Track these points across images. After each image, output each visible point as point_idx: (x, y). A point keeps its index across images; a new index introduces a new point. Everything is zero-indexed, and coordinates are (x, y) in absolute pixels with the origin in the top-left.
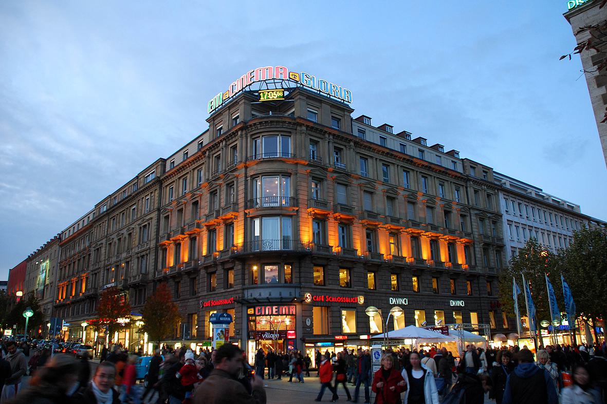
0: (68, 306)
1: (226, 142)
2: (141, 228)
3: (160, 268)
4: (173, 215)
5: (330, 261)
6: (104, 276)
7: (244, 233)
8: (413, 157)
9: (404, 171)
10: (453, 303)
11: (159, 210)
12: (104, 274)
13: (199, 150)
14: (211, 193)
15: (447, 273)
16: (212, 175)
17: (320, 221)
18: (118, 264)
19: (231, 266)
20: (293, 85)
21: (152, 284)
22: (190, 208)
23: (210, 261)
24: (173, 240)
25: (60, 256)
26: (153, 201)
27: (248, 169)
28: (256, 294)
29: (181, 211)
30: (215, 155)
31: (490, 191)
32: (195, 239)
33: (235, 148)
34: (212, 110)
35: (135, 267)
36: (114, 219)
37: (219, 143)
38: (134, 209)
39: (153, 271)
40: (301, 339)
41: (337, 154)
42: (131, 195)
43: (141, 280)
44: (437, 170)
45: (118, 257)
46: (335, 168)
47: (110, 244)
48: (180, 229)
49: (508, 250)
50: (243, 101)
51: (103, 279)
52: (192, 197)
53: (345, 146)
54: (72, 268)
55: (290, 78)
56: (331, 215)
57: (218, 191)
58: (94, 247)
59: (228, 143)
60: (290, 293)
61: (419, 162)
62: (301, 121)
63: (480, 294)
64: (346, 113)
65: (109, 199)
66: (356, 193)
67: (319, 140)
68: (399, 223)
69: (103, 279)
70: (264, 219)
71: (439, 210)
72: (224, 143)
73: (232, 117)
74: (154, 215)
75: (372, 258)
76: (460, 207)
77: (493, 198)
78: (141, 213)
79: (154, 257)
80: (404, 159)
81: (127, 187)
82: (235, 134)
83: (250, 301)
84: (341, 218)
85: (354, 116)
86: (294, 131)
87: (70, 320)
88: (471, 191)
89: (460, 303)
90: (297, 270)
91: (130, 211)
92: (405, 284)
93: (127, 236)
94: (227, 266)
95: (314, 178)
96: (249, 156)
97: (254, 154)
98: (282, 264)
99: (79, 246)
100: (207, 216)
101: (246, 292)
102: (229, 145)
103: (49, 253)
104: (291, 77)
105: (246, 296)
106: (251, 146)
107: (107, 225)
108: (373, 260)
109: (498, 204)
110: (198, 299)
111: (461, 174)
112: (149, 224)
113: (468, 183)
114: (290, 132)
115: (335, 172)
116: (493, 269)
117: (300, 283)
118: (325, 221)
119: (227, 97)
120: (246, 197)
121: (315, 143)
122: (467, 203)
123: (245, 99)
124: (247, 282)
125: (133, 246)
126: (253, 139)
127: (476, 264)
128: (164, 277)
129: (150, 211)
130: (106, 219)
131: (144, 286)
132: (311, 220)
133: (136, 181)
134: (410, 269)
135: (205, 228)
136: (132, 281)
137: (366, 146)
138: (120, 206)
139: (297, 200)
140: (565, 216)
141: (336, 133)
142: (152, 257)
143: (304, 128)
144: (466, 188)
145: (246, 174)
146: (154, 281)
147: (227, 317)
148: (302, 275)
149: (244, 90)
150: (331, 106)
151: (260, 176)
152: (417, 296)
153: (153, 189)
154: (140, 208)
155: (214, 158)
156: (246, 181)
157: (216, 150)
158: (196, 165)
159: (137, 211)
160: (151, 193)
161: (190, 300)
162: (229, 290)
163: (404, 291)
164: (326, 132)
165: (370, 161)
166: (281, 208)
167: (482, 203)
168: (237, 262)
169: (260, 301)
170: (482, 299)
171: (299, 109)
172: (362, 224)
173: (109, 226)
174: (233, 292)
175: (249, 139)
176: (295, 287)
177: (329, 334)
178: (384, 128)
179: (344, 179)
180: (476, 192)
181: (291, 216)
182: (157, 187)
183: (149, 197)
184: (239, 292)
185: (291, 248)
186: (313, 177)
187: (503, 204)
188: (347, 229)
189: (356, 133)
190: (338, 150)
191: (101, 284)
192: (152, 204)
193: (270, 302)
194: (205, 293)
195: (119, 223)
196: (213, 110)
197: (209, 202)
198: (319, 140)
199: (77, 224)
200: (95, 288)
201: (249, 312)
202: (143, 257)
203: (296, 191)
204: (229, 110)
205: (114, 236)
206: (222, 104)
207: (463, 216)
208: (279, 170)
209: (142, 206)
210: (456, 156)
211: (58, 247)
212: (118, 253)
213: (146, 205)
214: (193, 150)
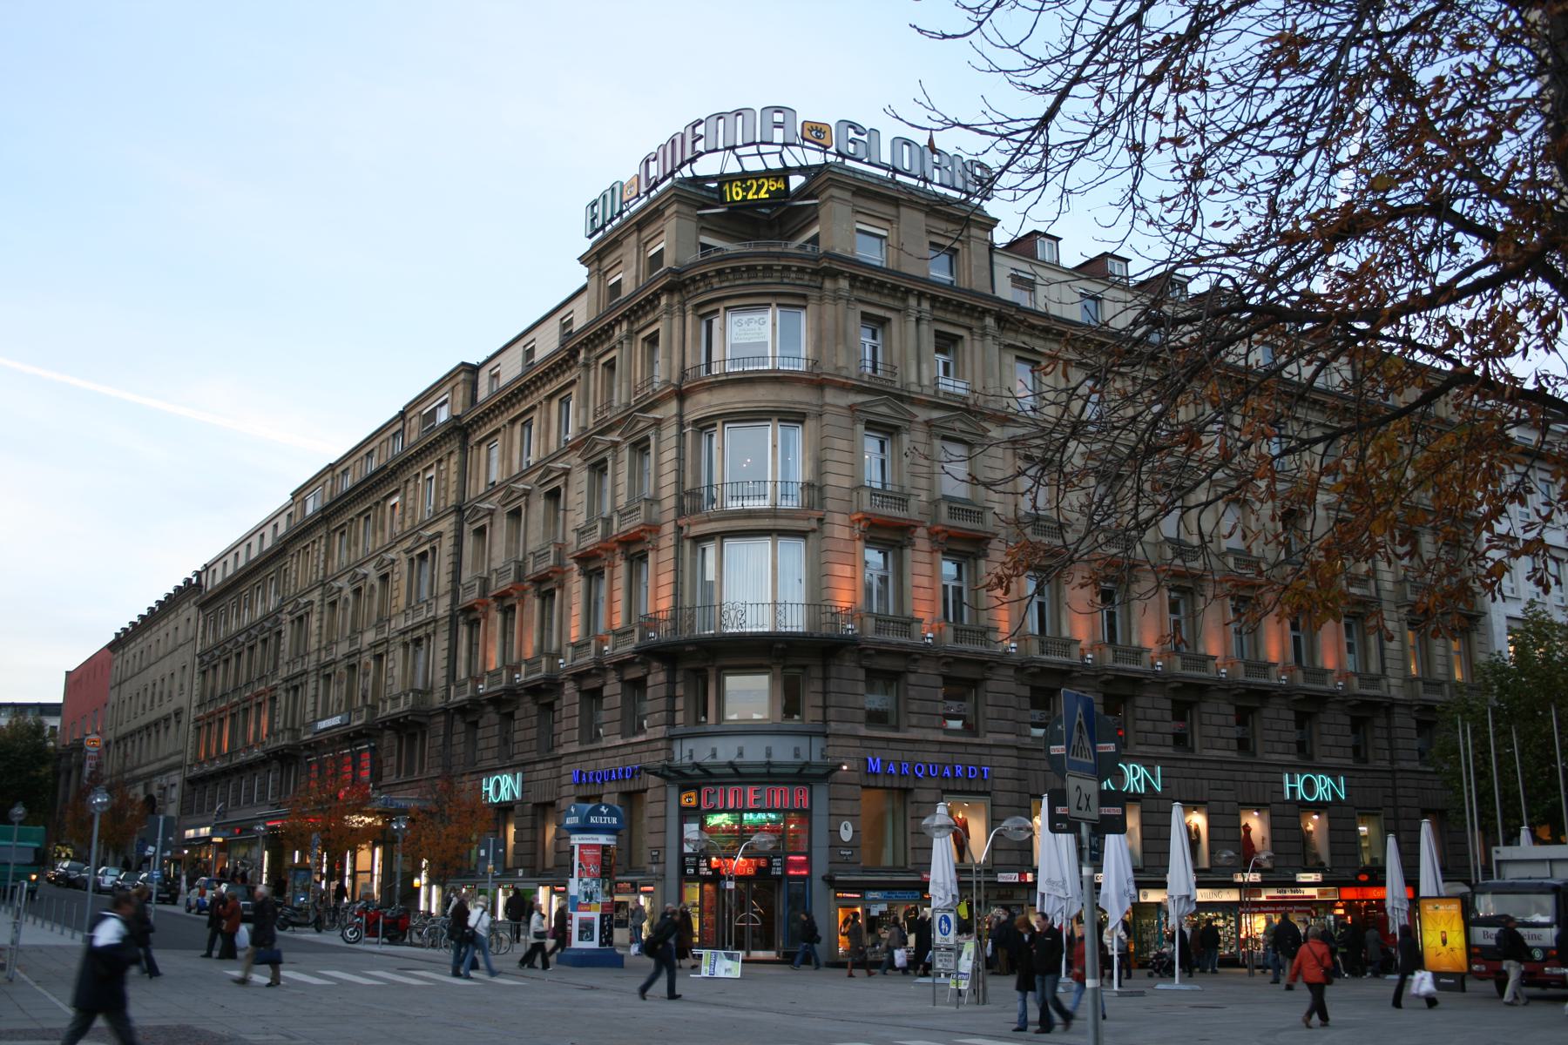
2: (412, 560)
4: (497, 526)
5: (916, 660)
6: (316, 696)
11: (459, 510)
12: (317, 689)
13: (563, 345)
22: (539, 506)
33: (653, 340)
35: (398, 672)
36: (343, 533)
39: (443, 683)
40: (823, 878)
42: (385, 467)
43: (413, 711)
45: (352, 641)
47: (333, 604)
48: (513, 566)
50: (674, 208)
51: (316, 703)
53: (970, 329)
54: (232, 672)
57: (610, 463)
58: (290, 613)
59: (636, 327)
60: (797, 749)
63: (1392, 761)
65: (329, 476)
66: (998, 463)
69: (316, 703)
70: (728, 543)
72: (625, 326)
74: (446, 525)
75: (1043, 652)
78: (413, 517)
79: (446, 644)
82: (652, 301)
83: (688, 772)
85: (1001, 237)
86: (815, 293)
91: (384, 511)
93: (377, 584)
95: (871, 426)
97: (703, 361)
102: (638, 332)
103: (172, 625)
104: (807, 135)
105: (677, 757)
106: (697, 339)
107: (323, 549)
108: (1045, 657)
112: (433, 549)
114: (804, 297)
116: (1440, 684)
117: (825, 721)
118: (901, 548)
120: (680, 482)
121: (877, 324)
124: (679, 717)
125: (394, 611)
127: (1384, 668)
129: (436, 513)
130: (322, 531)
131: (420, 724)
133: (399, 426)
134: (1164, 684)
136: (388, 710)
139: (821, 489)
142: (441, 643)
143: (844, 284)
146: (445, 711)
147: (608, 814)
148: (832, 699)
149: (678, 175)
151: (719, 423)
152: (1185, 764)
153: (444, 451)
154: (410, 504)
156: (681, 436)
157: (606, 346)
159: (404, 513)
160: (440, 461)
161: (540, 766)
162: (634, 740)
163: (1143, 748)
164: (908, 291)
166: (774, 513)
168: (655, 664)
169: (742, 770)
170: (1399, 775)
173: (329, 554)
174: (644, 747)
175: (689, 319)
177: (910, 867)
179: (963, 427)
182: (455, 445)
186: (868, 422)
189: (1005, 290)
191: (309, 718)
194: (575, 748)
195: (356, 545)
197: (585, 495)
199: (244, 545)
200: (293, 729)
201: (684, 802)
202: (418, 642)
203: (819, 465)
205: (343, 582)
208: (770, 406)
209: (415, 499)
211: (194, 609)
212: (353, 631)
213: (426, 495)
214: (547, 343)
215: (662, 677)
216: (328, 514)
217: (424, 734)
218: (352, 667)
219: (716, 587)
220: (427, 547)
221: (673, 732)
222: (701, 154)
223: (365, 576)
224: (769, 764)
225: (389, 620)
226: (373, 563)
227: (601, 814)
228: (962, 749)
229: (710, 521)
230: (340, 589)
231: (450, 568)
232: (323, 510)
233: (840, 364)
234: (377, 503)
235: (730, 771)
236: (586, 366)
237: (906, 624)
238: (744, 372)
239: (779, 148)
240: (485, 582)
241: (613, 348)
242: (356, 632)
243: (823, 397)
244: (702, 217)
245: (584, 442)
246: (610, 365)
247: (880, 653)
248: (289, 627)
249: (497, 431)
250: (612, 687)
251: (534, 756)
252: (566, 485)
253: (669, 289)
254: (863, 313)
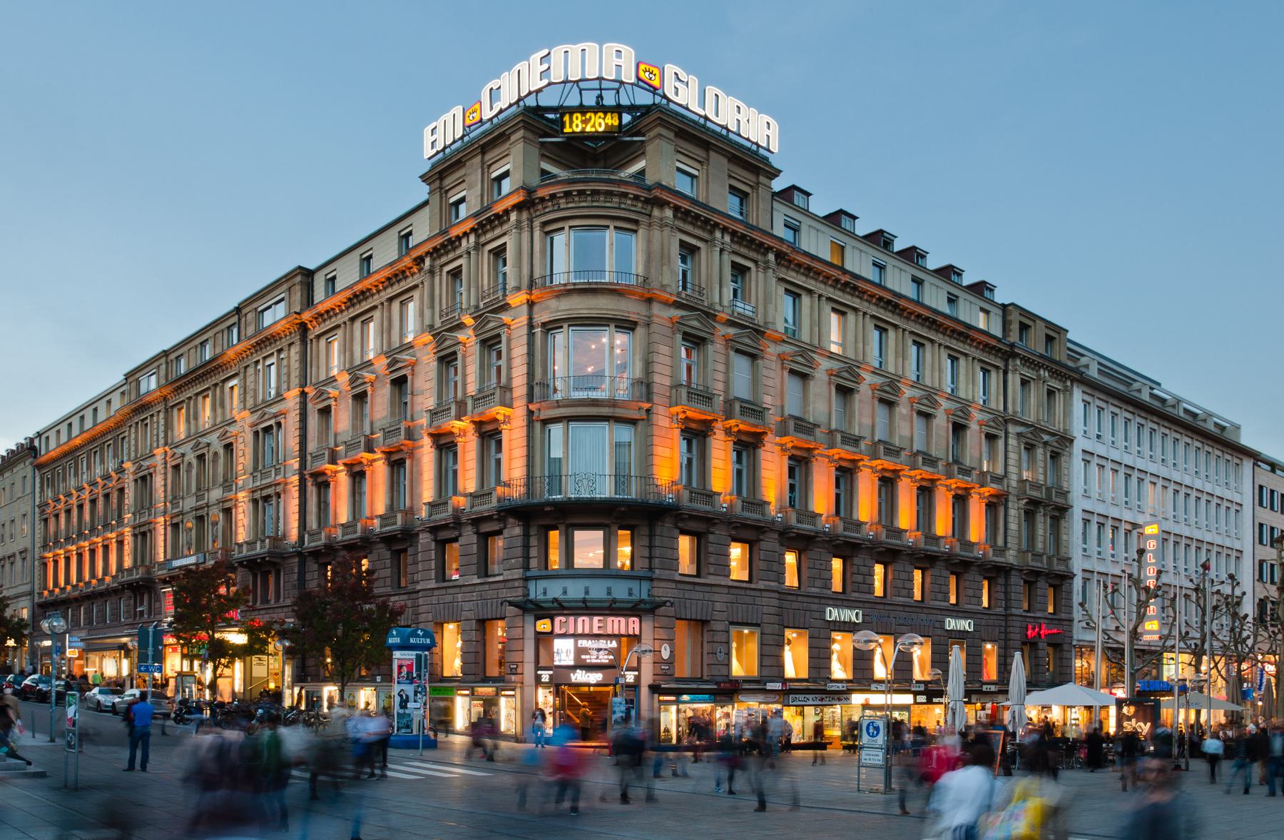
0: (75, 605)
1: (478, 236)
2: (256, 433)
3: (314, 526)
5: (715, 524)
7: (528, 456)
8: (900, 296)
9: (877, 327)
10: (952, 624)
14: (441, 360)
15: (946, 561)
16: (441, 316)
17: (696, 434)
18: (203, 512)
19: (497, 528)
20: (644, 98)
21: (296, 560)
23: (444, 516)
24: (345, 464)
25: (37, 490)
26: (284, 370)
27: (536, 308)
28: (554, 590)
29: (360, 398)
31: (1056, 384)
32: (401, 463)
34: (434, 151)
36: (180, 410)
37: (459, 238)
38: (232, 388)
41: (684, 261)
44: (946, 329)
45: (199, 498)
46: (732, 315)
48: (362, 440)
49: (1076, 517)
50: (521, 133)
52: (389, 365)
53: (756, 262)
55: (639, 79)
56: (719, 426)
59: (483, 240)
60: (630, 589)
61: (911, 307)
62: (665, 196)
63: (1006, 608)
64: (762, 179)
65: (163, 360)
66: (772, 374)
67: (699, 244)
68: (857, 446)
70: (572, 425)
71: (941, 422)
72: (472, 238)
73: (489, 174)
75: (799, 522)
76: (986, 417)
77: (1059, 398)
78: (255, 397)
80: (881, 299)
81: (210, 334)
84: (687, 418)
85: (778, 185)
87: (83, 634)
88: (1014, 381)
89: (965, 625)
90: (646, 542)
91: (222, 392)
92: (859, 578)
94: (486, 528)
96: (537, 274)
98: (614, 528)
99: (89, 468)
100: (434, 414)
101: (531, 585)
102: (483, 245)
104: (642, 75)
105: (532, 596)
106: (543, 252)
107: (162, 422)
109: (1068, 413)
110: (414, 596)
111: (999, 340)
113: (1010, 361)
114: (636, 222)
115: (731, 323)
117: (651, 569)
119: (477, 119)
120: (530, 374)
122: (1001, 408)
123: (525, 128)
126: (547, 233)
127: (1006, 543)
128: (325, 546)
131: (274, 564)
132: (677, 432)
133: (235, 319)
135: (427, 442)
137: (799, 265)
138: (196, 378)
140: (1207, 448)
141: (740, 229)
143: (669, 213)
144: (1005, 373)
145: (530, 319)
146: (299, 554)
147: (424, 636)
148: (657, 552)
150: (730, 160)
154: (250, 385)
155: (444, 273)
156: (531, 335)
157: (451, 256)
158: (397, 289)
160: (280, 351)
164: (716, 225)
165: (891, 333)
167: (1033, 409)
168: (511, 520)
171: (661, 165)
172: (781, 445)
174: (501, 585)
175: (537, 233)
176: (640, 578)
178: (834, 219)
180: (1024, 383)
181: (633, 422)
183: (273, 360)
184: (516, 584)
185: (633, 493)
186: (685, 334)
187: (1080, 416)
188: (748, 457)
189: (780, 231)
190: (739, 271)
191: (161, 558)
192: (284, 378)
193: (587, 608)
194: (433, 584)
196: (438, 152)
198: (699, 244)
204: (483, 153)
206: (462, 138)
207: (991, 438)
209: (256, 382)
210: (987, 294)
211: (29, 469)
212: (199, 489)
218: (200, 519)
219: (564, 462)
221: (528, 574)
223: (209, 445)
226: (217, 434)
227: (418, 636)
228: (743, 592)
230: (183, 455)
233: (665, 282)
234: (216, 385)
237: (711, 496)
238: (589, 283)
239: (617, 85)
241: (460, 257)
242: (201, 491)
243: (650, 309)
244: (543, 144)
247: (692, 517)
248: (132, 484)
249: (338, 327)
254: (681, 241)
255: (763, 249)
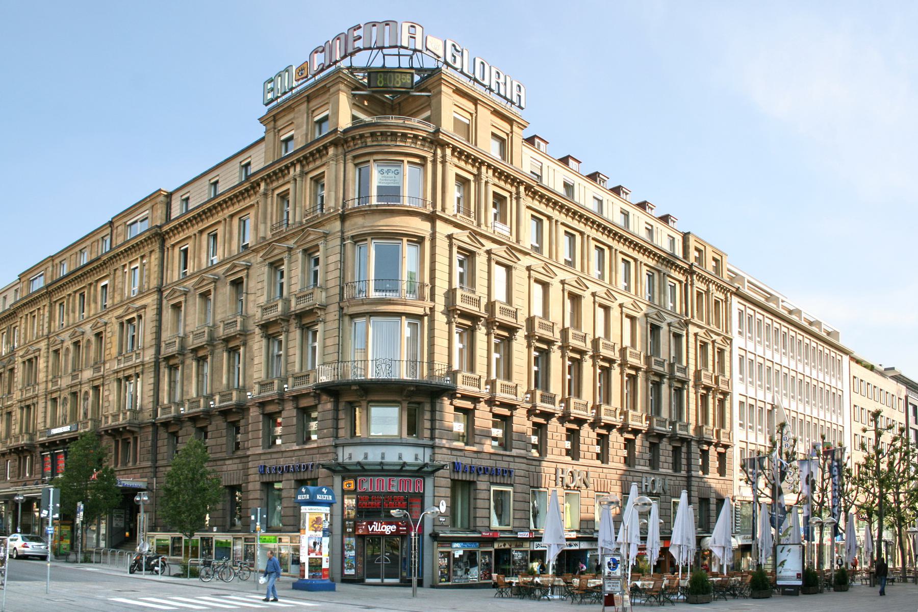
2: (122, 324)
4: (190, 302)
12: (46, 407)
30: (277, 192)
37: (287, 167)
40: (430, 535)
42: (98, 259)
47: (57, 352)
51: (45, 417)
58: (22, 357)
65: (50, 264)
72: (298, 168)
74: (151, 300)
78: (122, 294)
79: (152, 381)
91: (96, 290)
102: (307, 173)
107: (47, 314)
112: (140, 317)
124: (342, 433)
130: (46, 302)
131: (132, 432)
142: (149, 379)
145: (343, 232)
153: (147, 250)
155: (275, 196)
156: (343, 246)
159: (114, 291)
160: (143, 257)
161: (227, 462)
169: (366, 467)
182: (156, 246)
194: (260, 450)
195: (74, 312)
197: (265, 284)
209: (124, 282)
212: (74, 370)
213: (133, 279)
214: (230, 179)
215: (329, 406)
216: (49, 291)
217: (136, 439)
218: (74, 394)
220: (135, 315)
221: (338, 442)
222: (359, 50)
223: (83, 333)
224: (381, 464)
225: (104, 363)
227: (323, 493)
229: (363, 304)
231: (154, 330)
232: (47, 287)
234: (91, 284)
235: (359, 468)
236: (265, 194)
239: (411, 52)
240: (183, 339)
241: (288, 182)
245: (265, 245)
246: (284, 197)
248: (21, 366)
250: (290, 411)
251: (224, 455)
252: (248, 276)
253: (335, 143)
255: (515, 181)
